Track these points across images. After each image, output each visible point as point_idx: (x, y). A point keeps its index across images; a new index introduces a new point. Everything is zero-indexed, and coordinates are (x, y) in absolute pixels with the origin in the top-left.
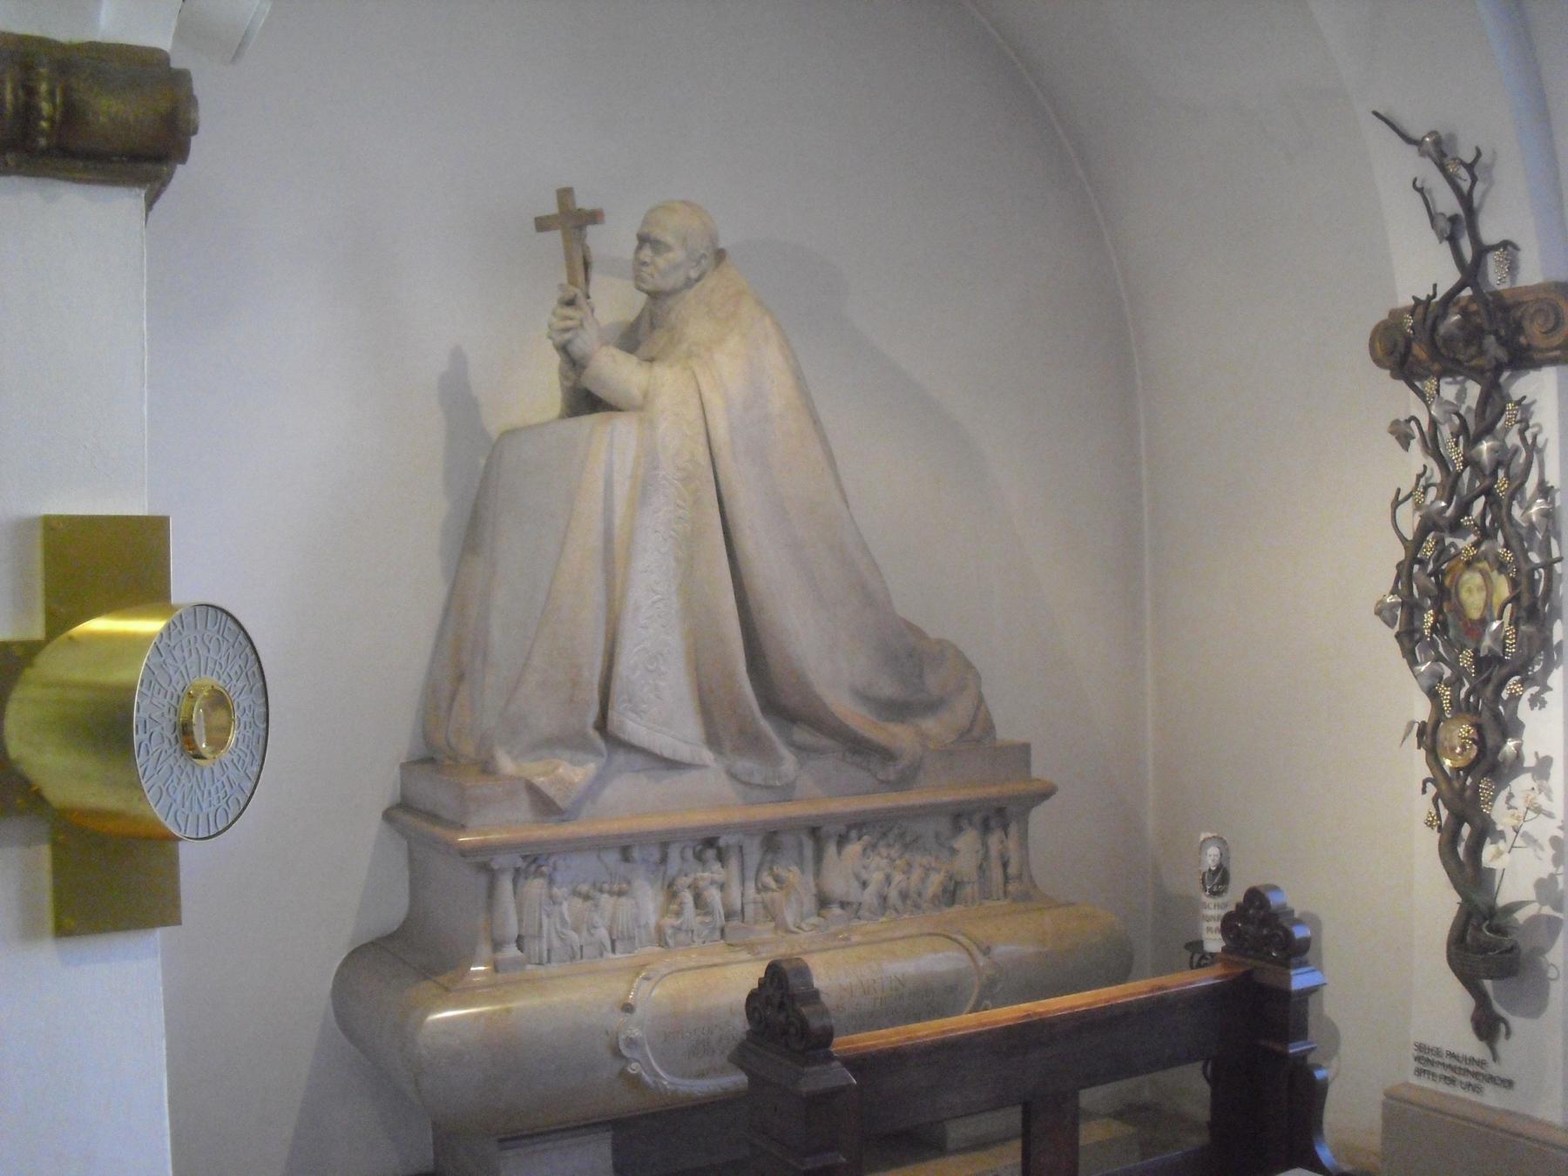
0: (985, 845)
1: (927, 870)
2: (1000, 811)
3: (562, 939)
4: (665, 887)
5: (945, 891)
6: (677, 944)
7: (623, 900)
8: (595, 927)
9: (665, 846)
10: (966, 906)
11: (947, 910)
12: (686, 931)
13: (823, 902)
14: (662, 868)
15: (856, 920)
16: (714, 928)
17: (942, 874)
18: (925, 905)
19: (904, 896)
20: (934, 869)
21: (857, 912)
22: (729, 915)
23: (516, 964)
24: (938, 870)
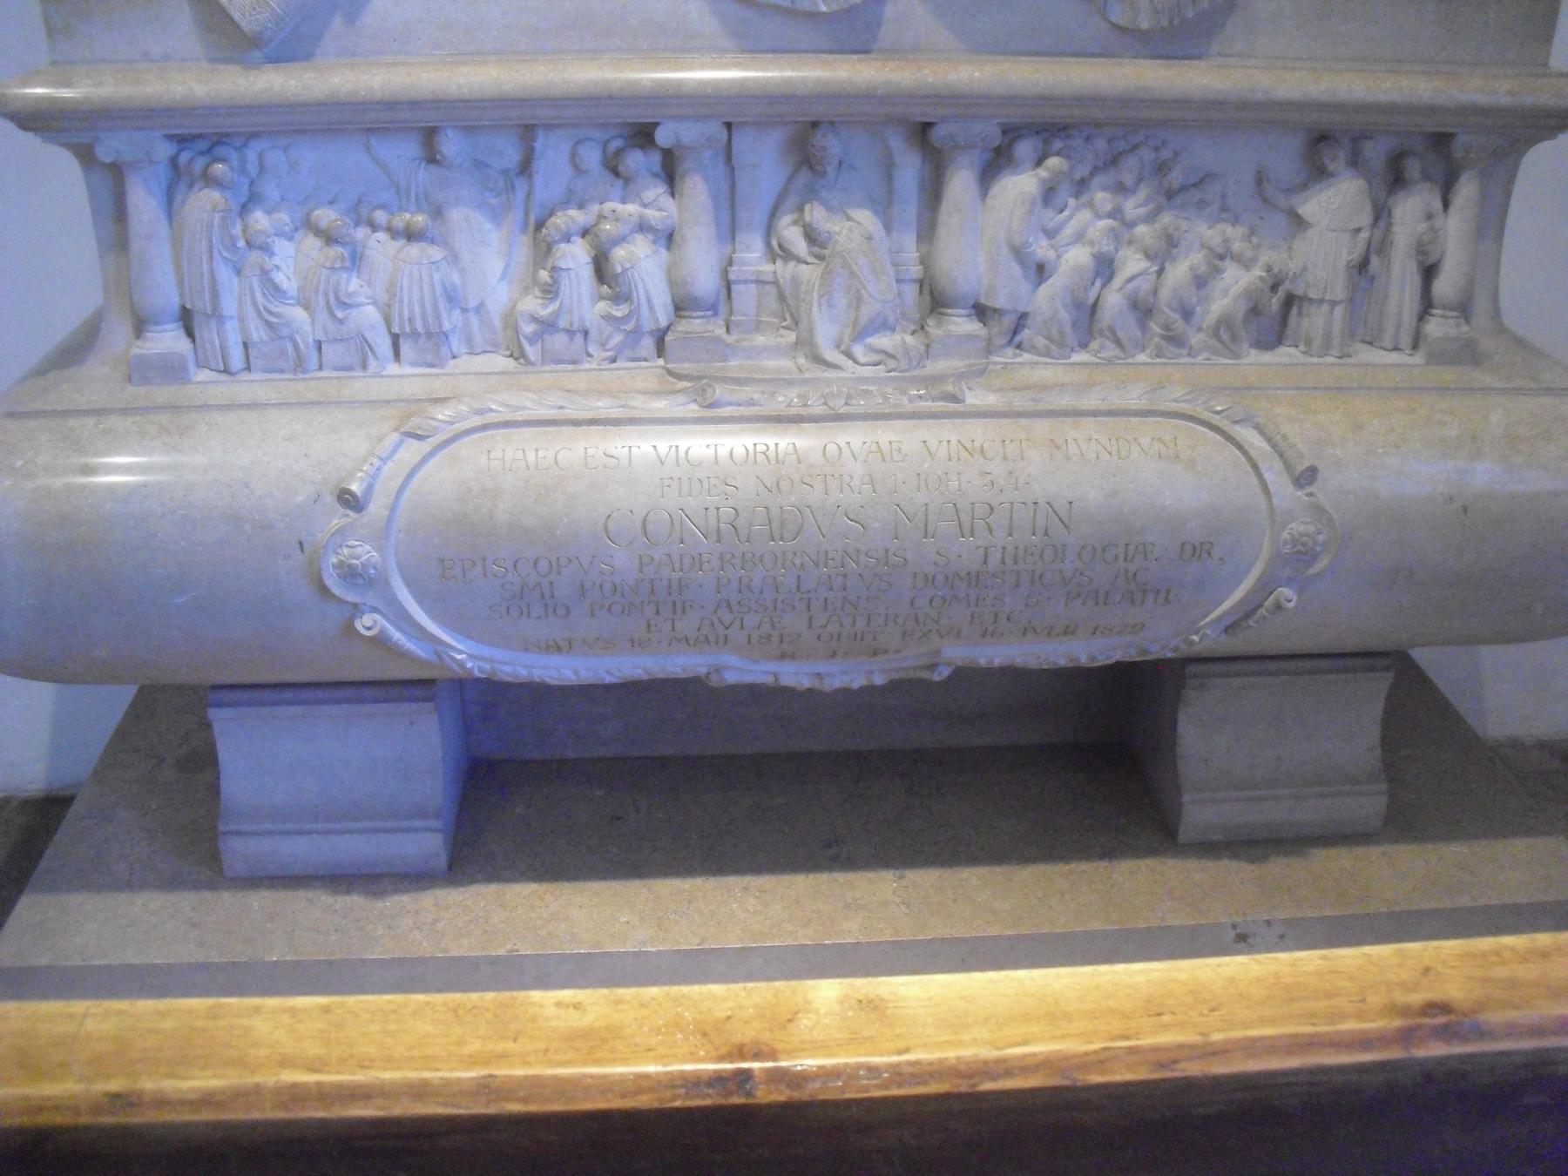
0: (1381, 214)
1: (1221, 256)
2: (1441, 141)
3: (267, 323)
4: (531, 228)
5: (1254, 311)
6: (550, 358)
7: (414, 250)
8: (345, 305)
9: (528, 133)
10: (1304, 353)
11: (1254, 356)
12: (570, 333)
13: (936, 300)
14: (521, 185)
15: (1010, 351)
16: (636, 333)
17: (1257, 272)
18: (1196, 339)
19: (1143, 310)
20: (1238, 259)
21: (1015, 332)
22: (681, 307)
23: (173, 370)
24: (1246, 263)
